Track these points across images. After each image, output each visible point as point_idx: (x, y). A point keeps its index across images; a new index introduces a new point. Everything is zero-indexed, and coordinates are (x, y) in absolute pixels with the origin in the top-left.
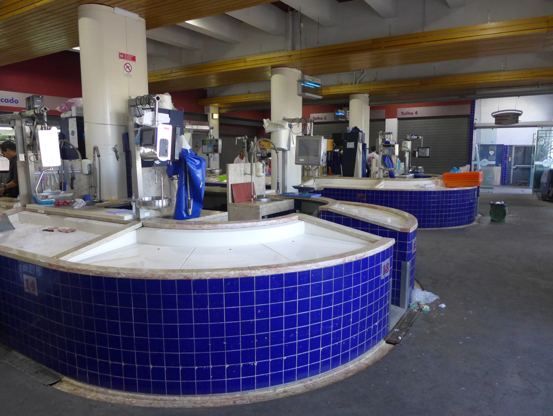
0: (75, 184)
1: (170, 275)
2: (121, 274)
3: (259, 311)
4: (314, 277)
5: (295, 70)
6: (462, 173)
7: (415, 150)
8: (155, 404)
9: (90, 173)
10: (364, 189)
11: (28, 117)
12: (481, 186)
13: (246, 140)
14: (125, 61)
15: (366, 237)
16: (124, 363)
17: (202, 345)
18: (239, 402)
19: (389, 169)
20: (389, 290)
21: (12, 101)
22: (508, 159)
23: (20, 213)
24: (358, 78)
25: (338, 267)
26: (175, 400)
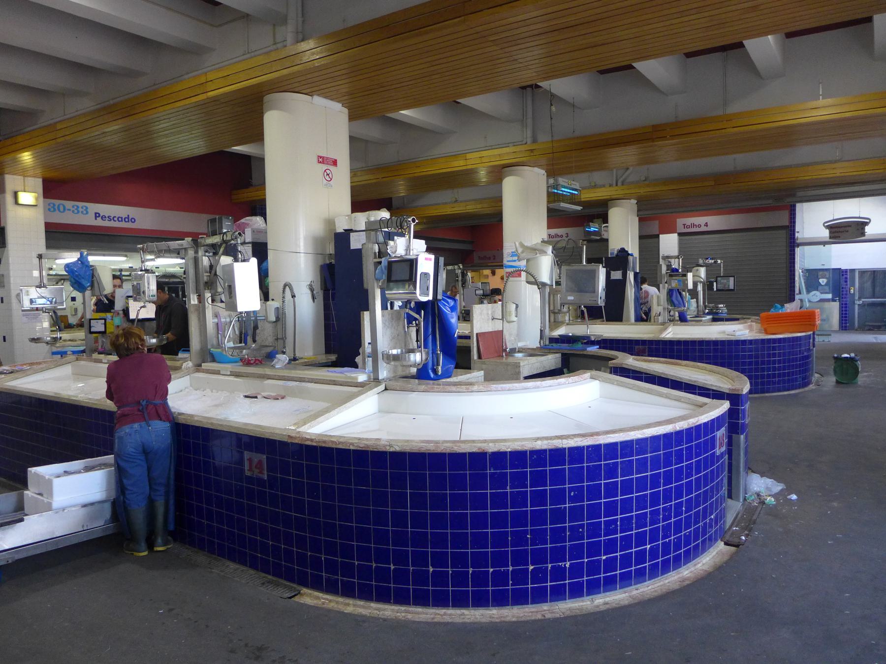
0: (258, 336)
1: (459, 446)
2: (394, 446)
3: (572, 494)
4: (639, 449)
5: (536, 170)
6: (791, 313)
7: (712, 280)
8: (438, 619)
9: (278, 319)
10: (645, 339)
11: (207, 245)
12: (817, 333)
13: (460, 271)
14: (325, 167)
15: (690, 399)
16: (394, 565)
17: (500, 540)
18: (548, 616)
19: (680, 309)
20: (722, 473)
21: (127, 220)
22: (850, 290)
23: (192, 375)
24: (620, 178)
25: (667, 436)
26: (463, 614)
